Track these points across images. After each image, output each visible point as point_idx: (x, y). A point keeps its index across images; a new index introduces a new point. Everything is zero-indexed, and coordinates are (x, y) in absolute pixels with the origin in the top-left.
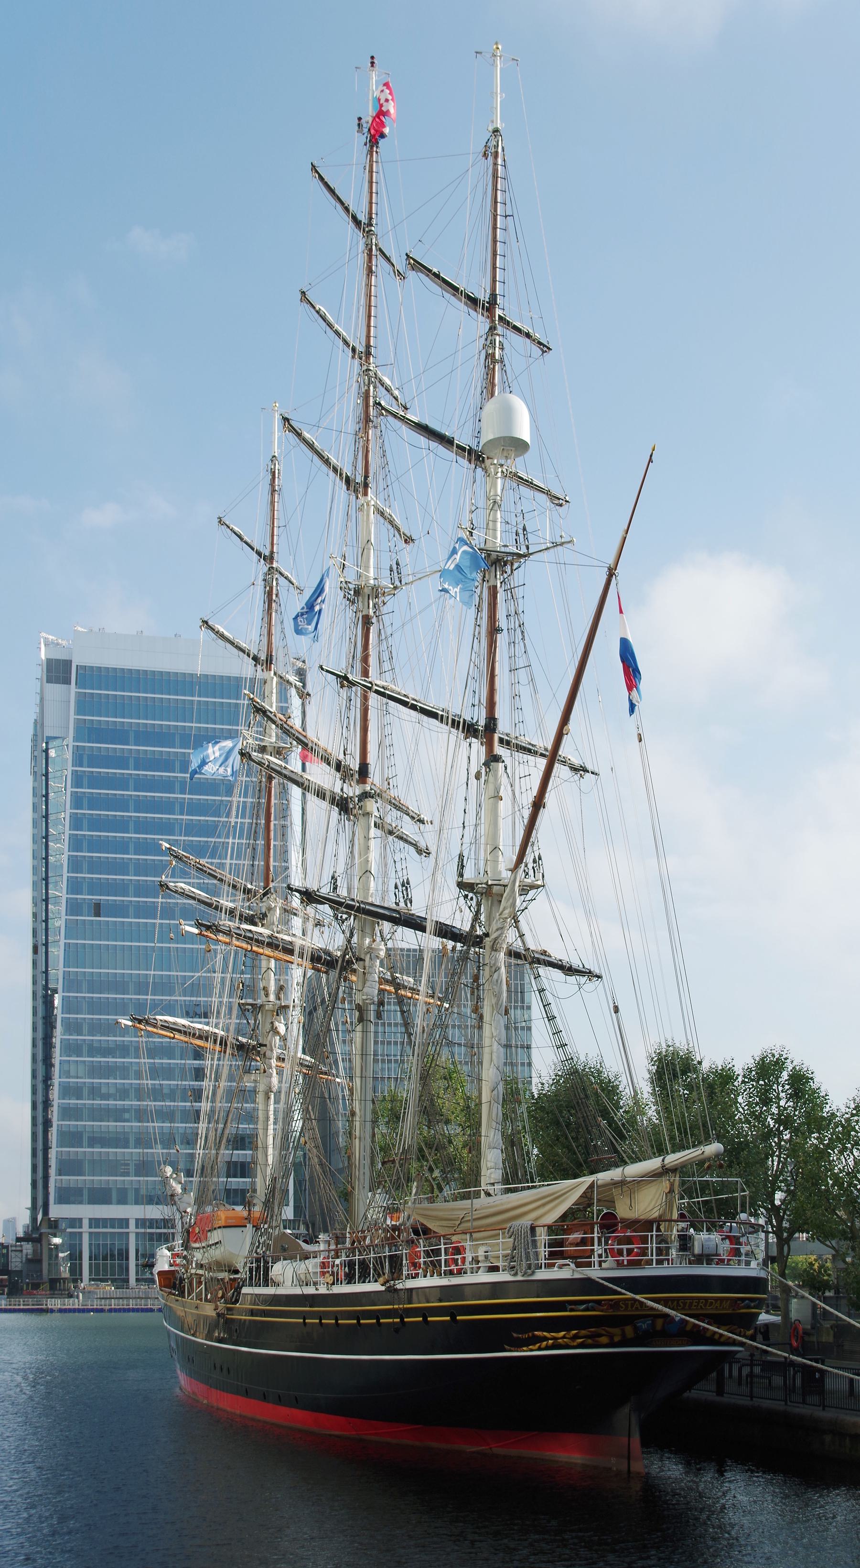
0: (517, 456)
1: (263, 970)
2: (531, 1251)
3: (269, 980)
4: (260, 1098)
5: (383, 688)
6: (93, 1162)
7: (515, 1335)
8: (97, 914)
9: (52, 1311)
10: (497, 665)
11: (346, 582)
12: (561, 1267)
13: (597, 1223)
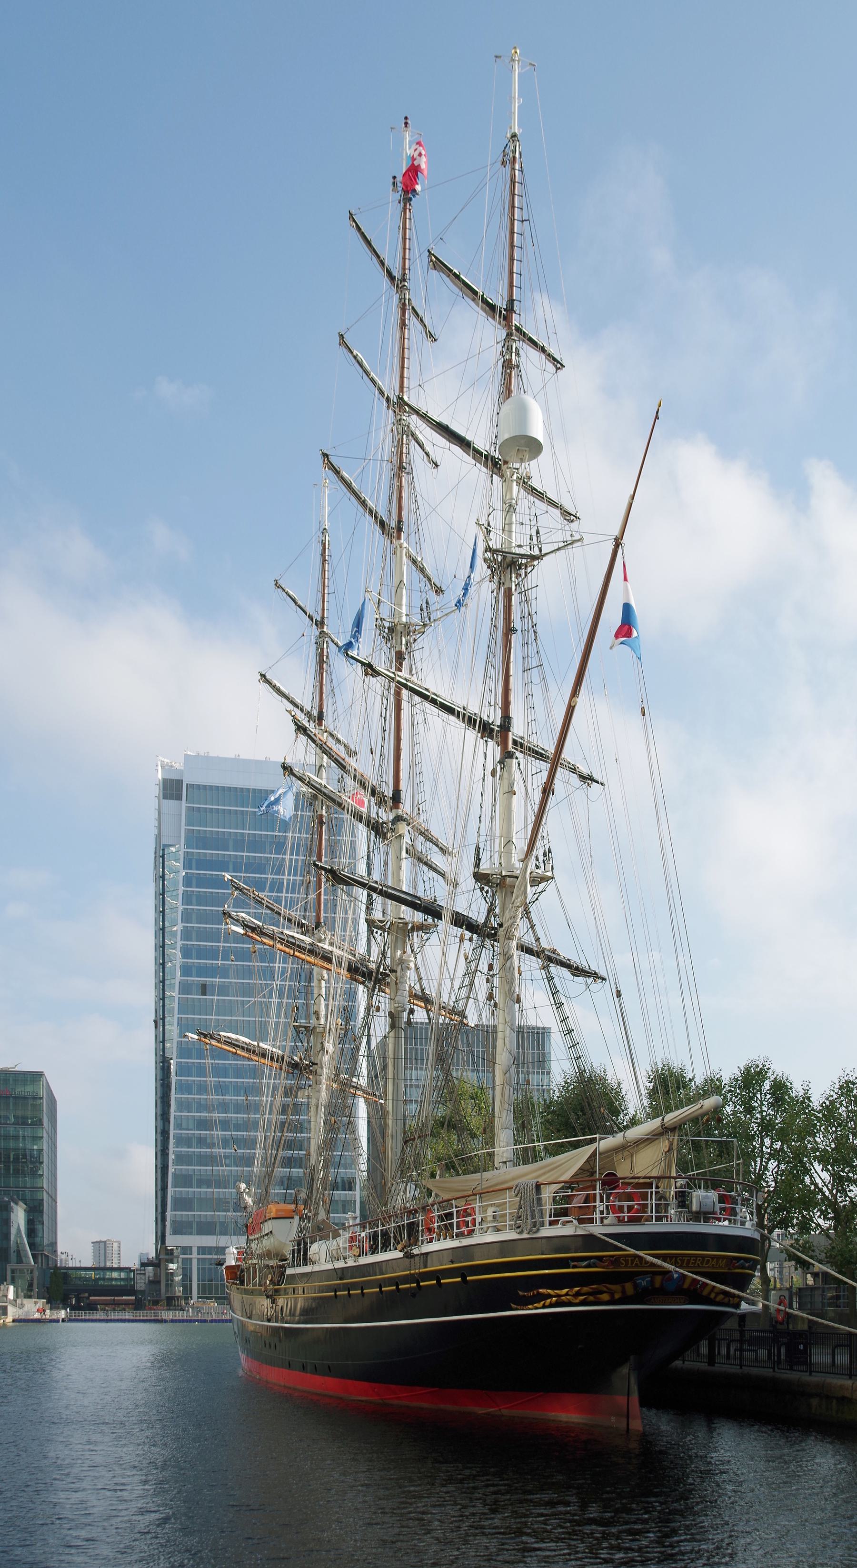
0: (531, 459)
1: (315, 996)
2: (536, 1209)
3: (320, 1005)
4: (313, 1110)
5: (406, 679)
6: (200, 1200)
7: (521, 1293)
8: (204, 994)
9: (165, 1321)
10: (512, 665)
11: (382, 619)
12: (565, 1223)
13: (599, 1180)
